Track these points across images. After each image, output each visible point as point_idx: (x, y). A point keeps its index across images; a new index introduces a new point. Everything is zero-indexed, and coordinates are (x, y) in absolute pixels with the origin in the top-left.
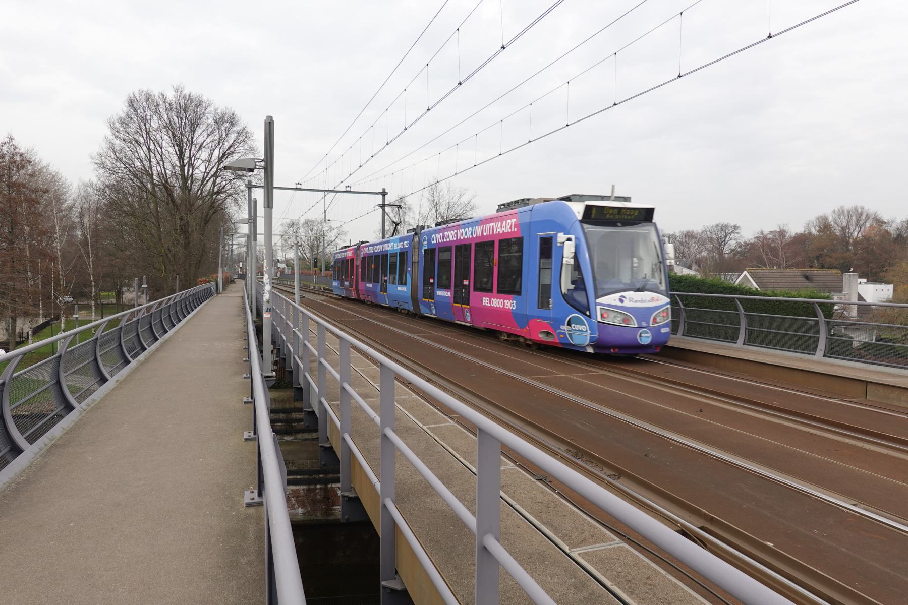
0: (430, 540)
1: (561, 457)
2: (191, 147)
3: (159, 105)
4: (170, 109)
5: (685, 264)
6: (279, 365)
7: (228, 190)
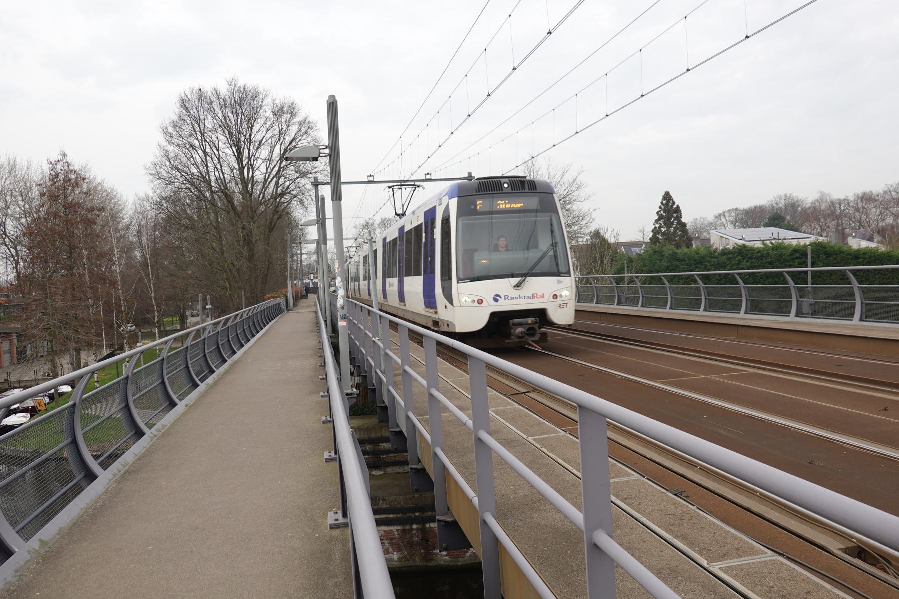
0: (538, 556)
1: (700, 468)
2: (250, 146)
3: (212, 102)
4: (223, 106)
5: (863, 234)
6: (361, 389)
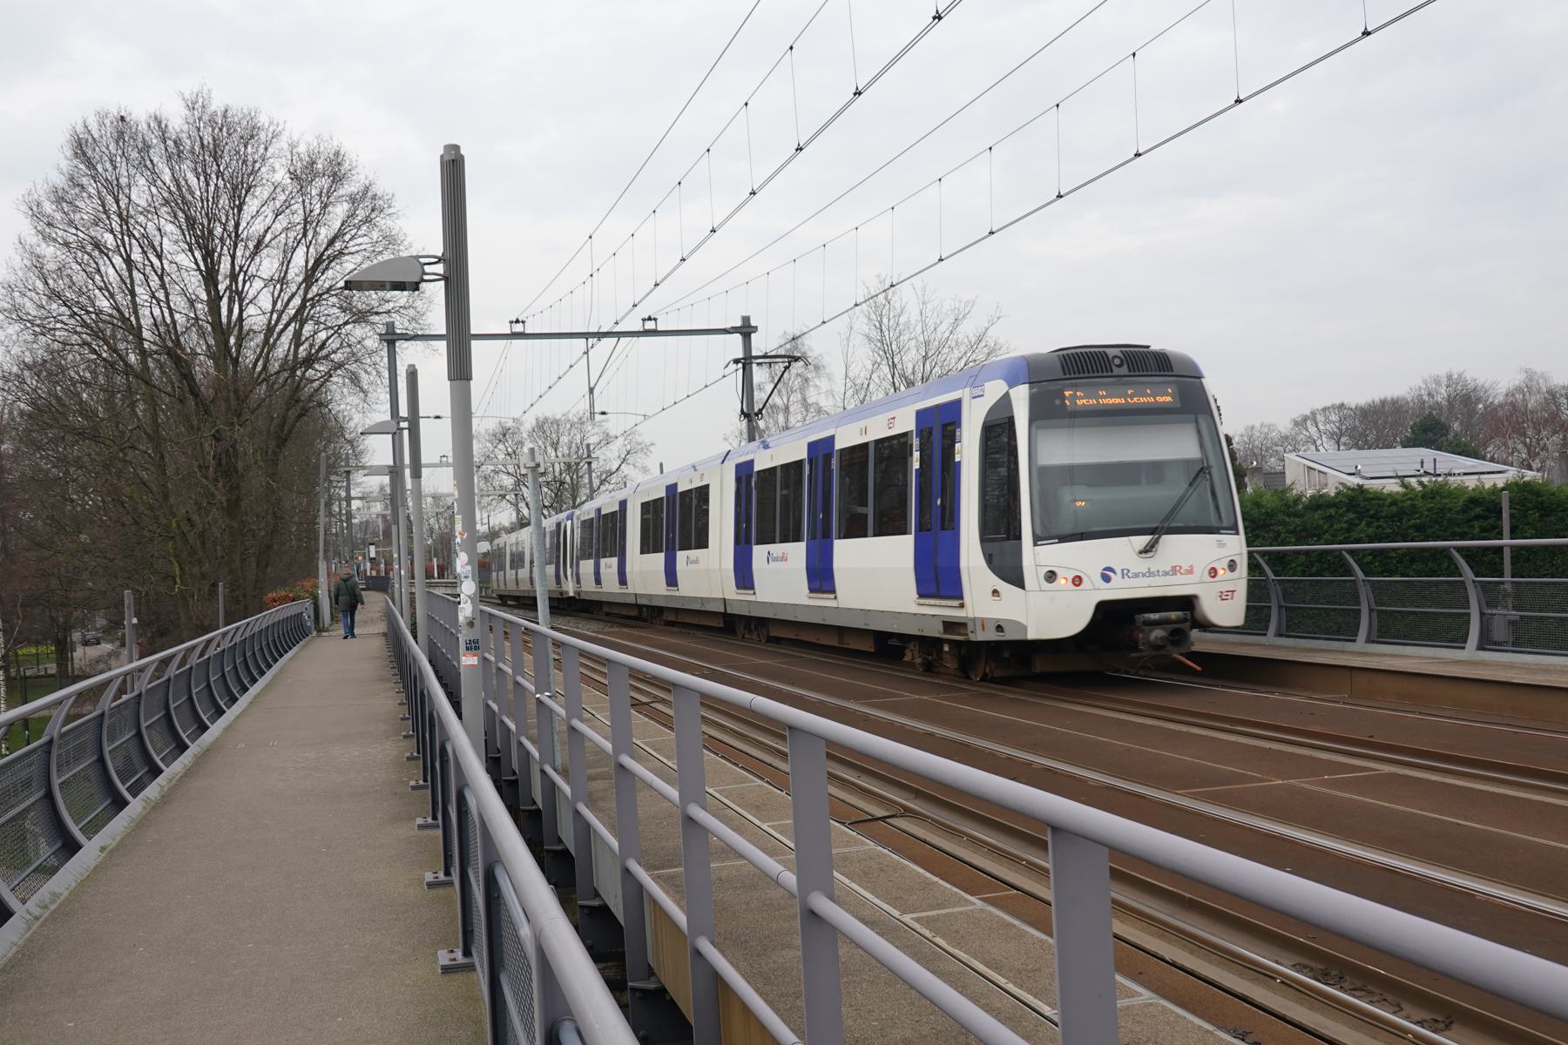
1: (1282, 982)
3: (149, 147)
4: (176, 154)
7: (334, 352)
